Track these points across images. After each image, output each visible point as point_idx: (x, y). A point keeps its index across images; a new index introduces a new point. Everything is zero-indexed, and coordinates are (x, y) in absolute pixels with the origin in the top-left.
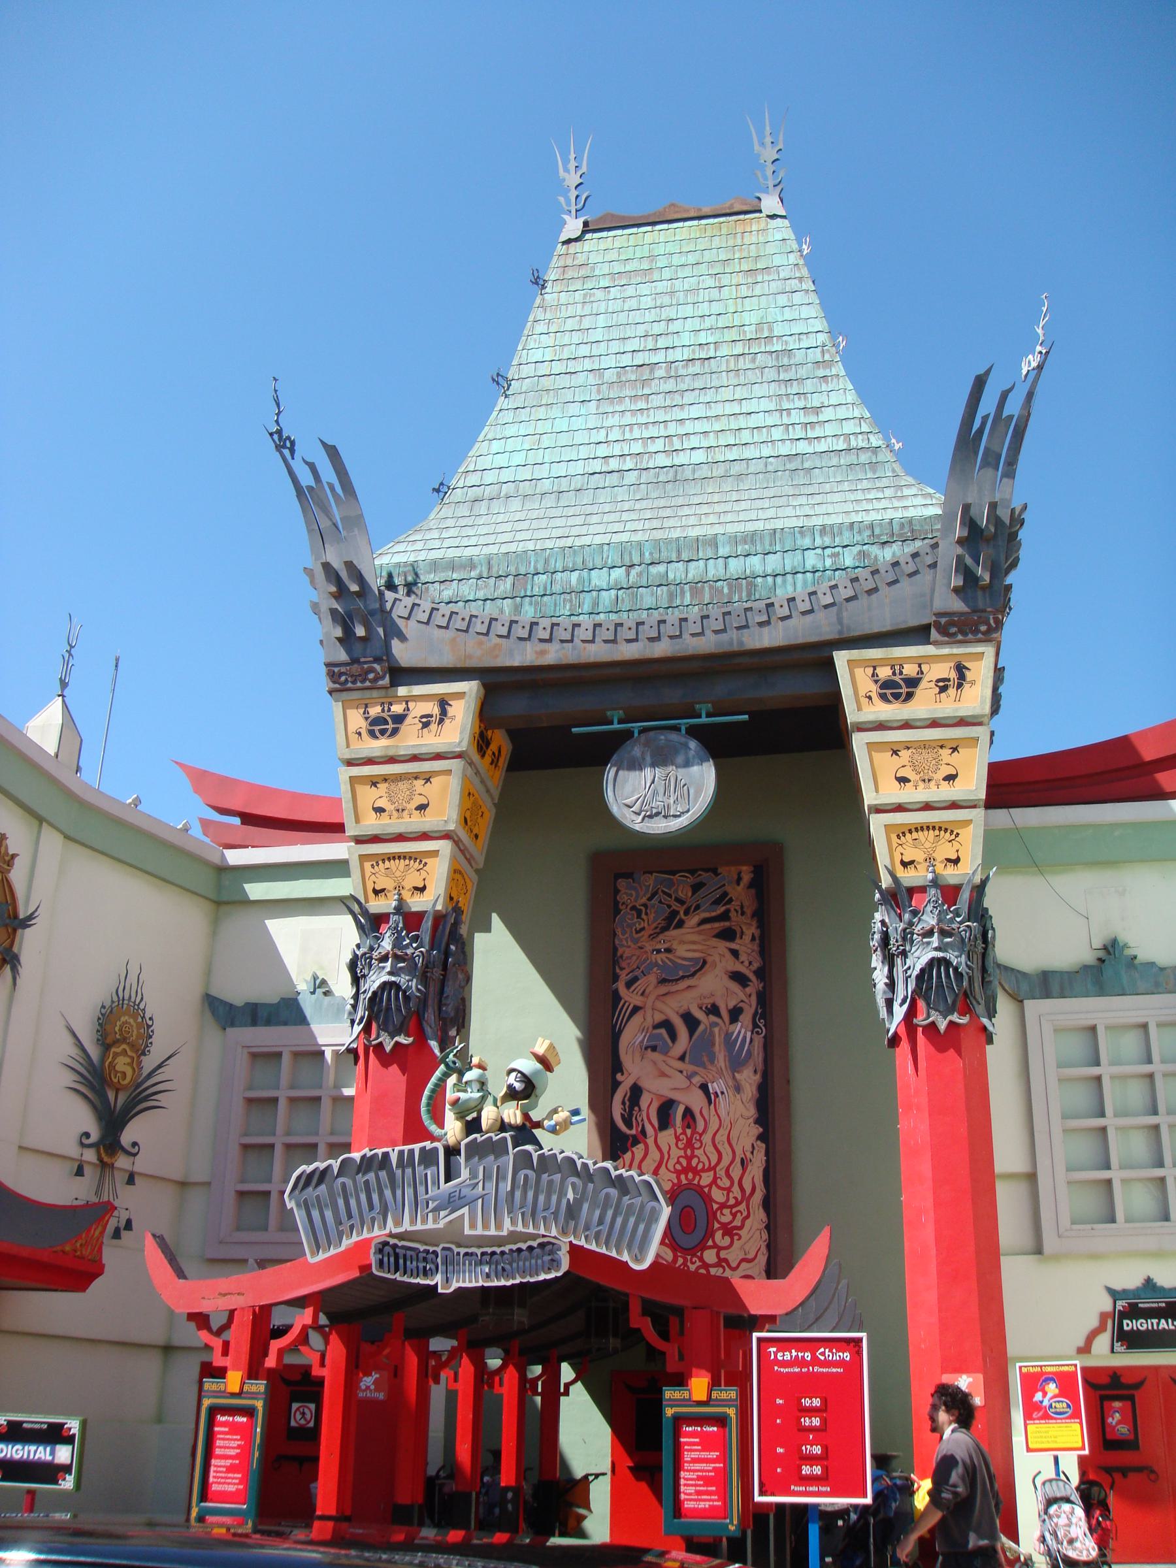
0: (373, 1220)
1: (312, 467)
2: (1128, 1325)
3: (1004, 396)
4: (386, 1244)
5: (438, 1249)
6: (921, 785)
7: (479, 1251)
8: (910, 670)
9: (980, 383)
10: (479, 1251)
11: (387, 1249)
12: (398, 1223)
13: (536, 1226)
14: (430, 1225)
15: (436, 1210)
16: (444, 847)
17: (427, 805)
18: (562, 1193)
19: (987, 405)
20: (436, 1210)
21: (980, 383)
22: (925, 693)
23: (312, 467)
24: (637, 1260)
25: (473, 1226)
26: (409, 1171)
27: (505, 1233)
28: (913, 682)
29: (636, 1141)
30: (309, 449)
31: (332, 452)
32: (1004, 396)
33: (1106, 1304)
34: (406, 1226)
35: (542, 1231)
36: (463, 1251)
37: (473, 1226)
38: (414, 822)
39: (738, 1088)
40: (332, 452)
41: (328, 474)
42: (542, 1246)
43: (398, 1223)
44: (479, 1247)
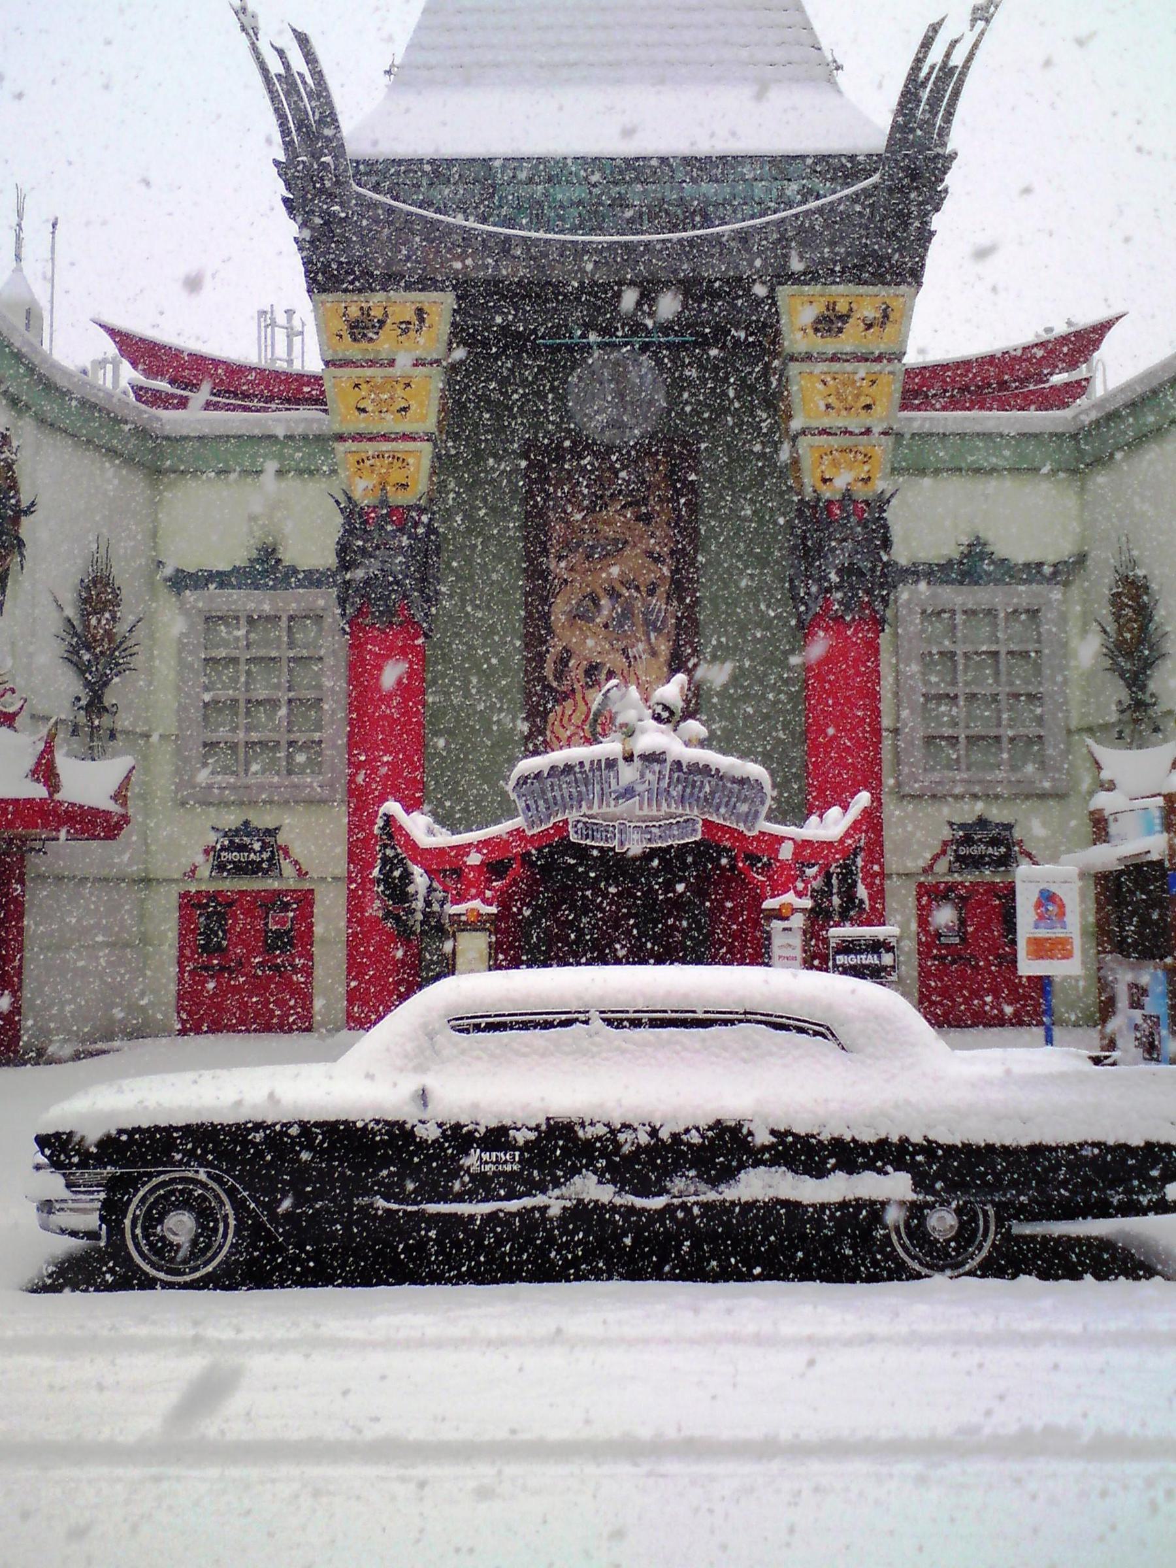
0: (572, 807)
1: (281, 53)
2: (963, 851)
3: (954, 44)
4: (578, 821)
5: (616, 824)
6: (844, 413)
7: (644, 825)
8: (842, 308)
9: (935, 28)
10: (644, 825)
11: (580, 825)
12: (590, 808)
13: (684, 809)
14: (612, 809)
15: (617, 798)
16: (427, 447)
17: (409, 408)
18: (702, 787)
19: (935, 56)
20: (617, 798)
21: (935, 28)
22: (853, 328)
23: (281, 53)
24: (749, 830)
25: (641, 809)
26: (598, 773)
27: (662, 813)
28: (844, 318)
29: (566, 696)
30: (274, 33)
31: (303, 40)
32: (954, 44)
33: (946, 833)
34: (595, 810)
35: (688, 812)
36: (633, 825)
37: (641, 809)
38: (391, 423)
39: (654, 653)
40: (303, 40)
41: (298, 64)
42: (686, 821)
43: (590, 808)
44: (644, 821)
